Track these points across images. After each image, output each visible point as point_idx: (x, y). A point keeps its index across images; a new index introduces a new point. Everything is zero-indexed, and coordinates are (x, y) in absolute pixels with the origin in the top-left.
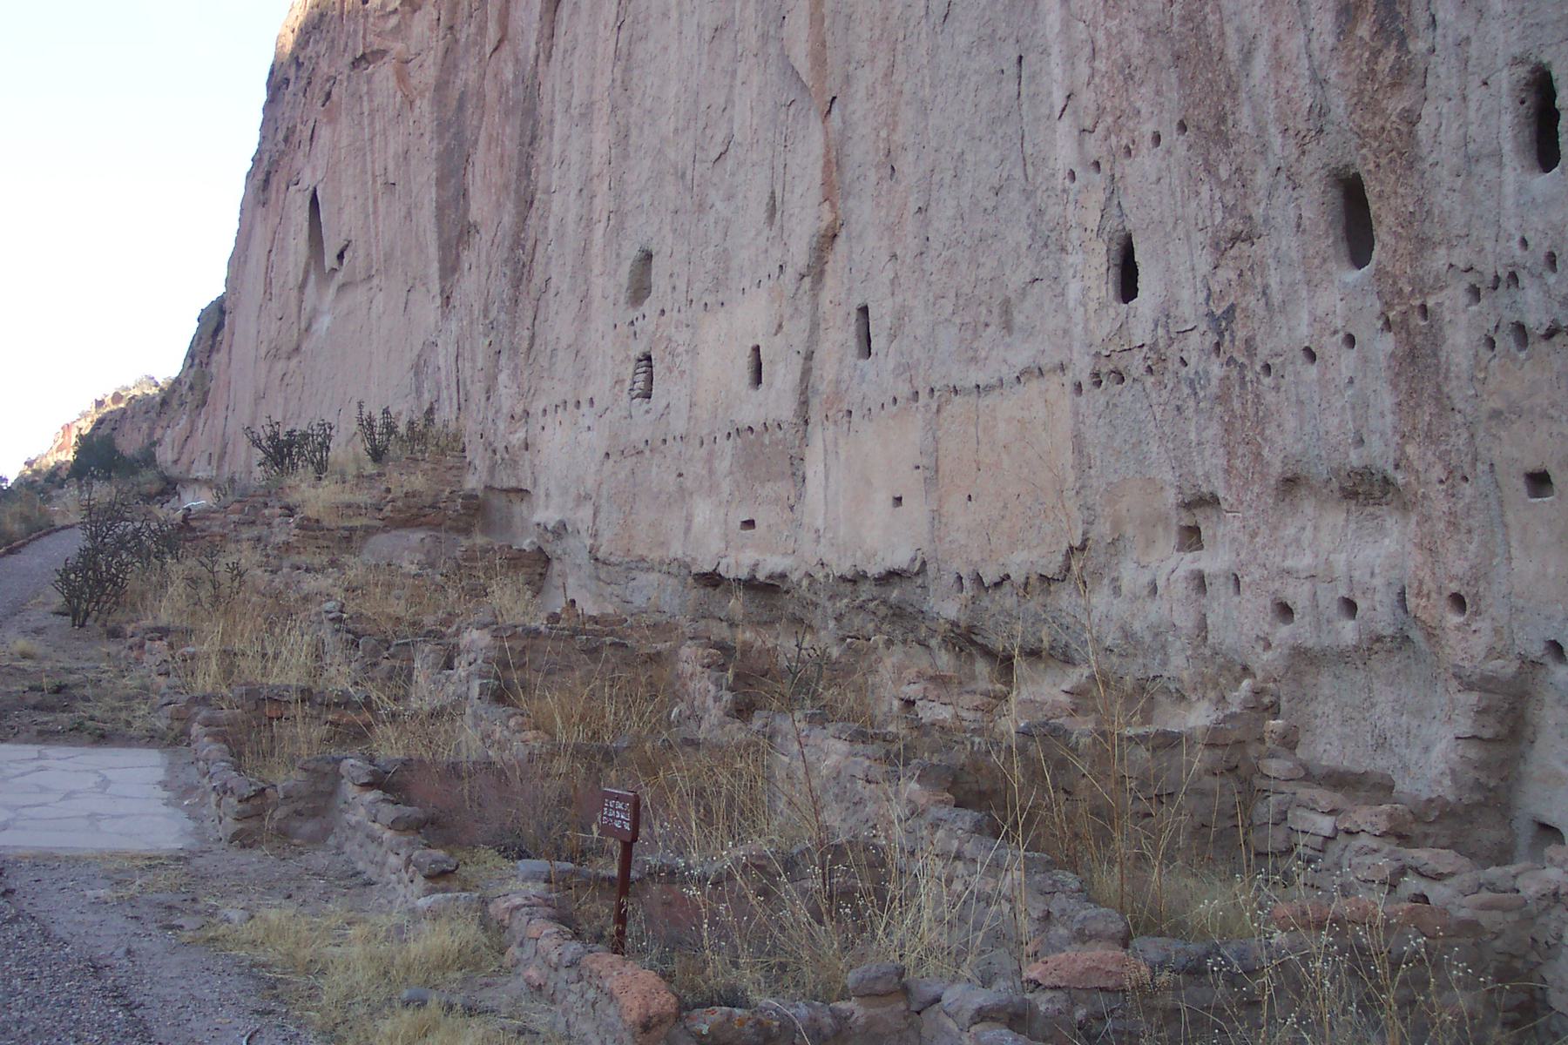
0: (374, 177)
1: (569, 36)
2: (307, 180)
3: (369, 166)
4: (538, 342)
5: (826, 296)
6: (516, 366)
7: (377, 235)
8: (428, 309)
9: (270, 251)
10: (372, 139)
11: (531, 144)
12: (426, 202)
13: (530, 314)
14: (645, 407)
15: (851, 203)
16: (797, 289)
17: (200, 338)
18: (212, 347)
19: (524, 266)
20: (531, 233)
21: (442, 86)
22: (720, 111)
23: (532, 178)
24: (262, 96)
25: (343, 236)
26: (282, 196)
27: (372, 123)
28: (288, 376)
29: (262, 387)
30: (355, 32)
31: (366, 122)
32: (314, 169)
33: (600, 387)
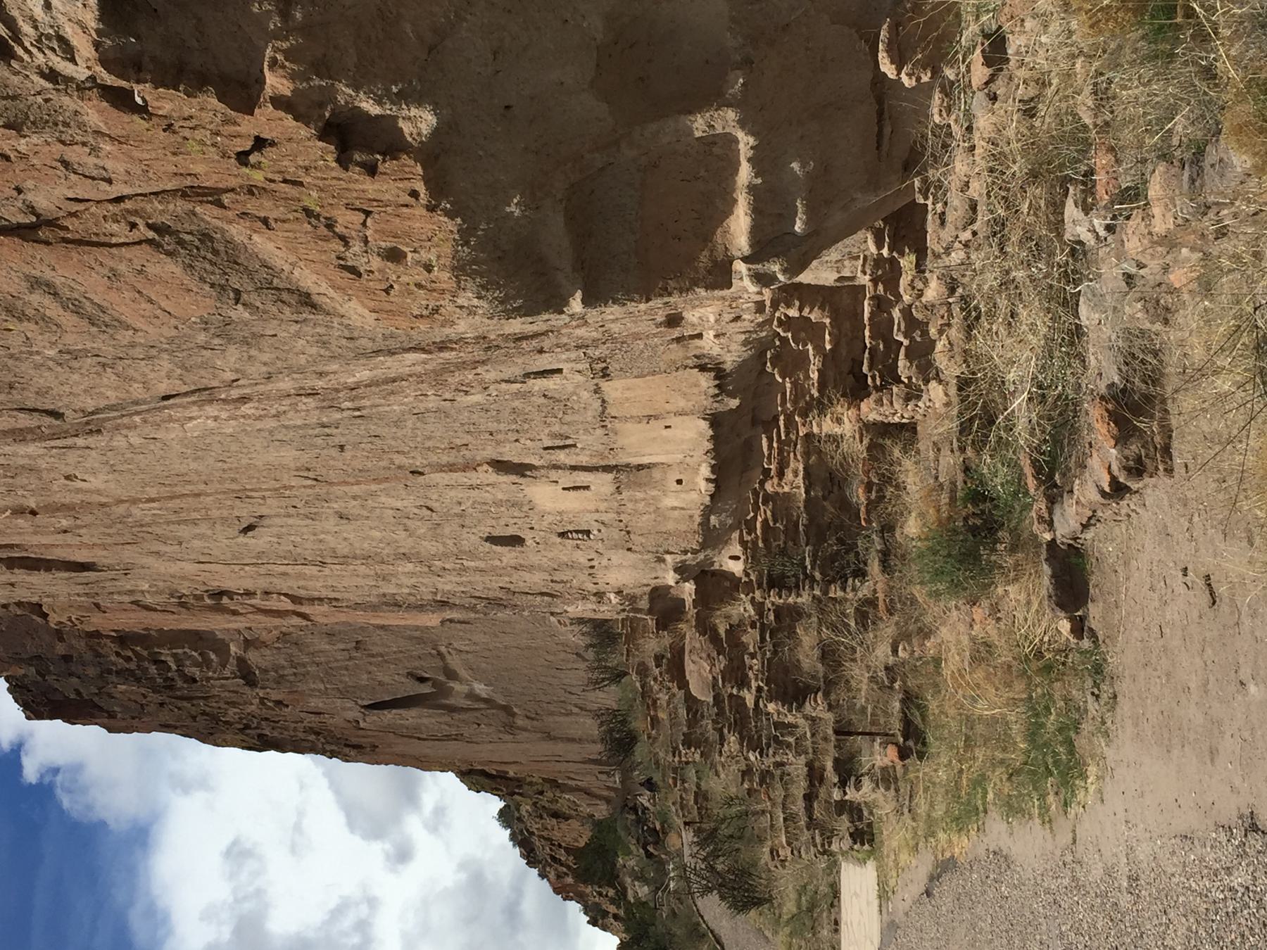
0: (351, 658)
1: (321, 589)
2: (354, 714)
4: (544, 590)
5: (536, 462)
9: (419, 739)
15: (478, 458)
17: (493, 789)
18: (501, 777)
24: (272, 755)
26: (370, 733)
27: (304, 665)
28: (528, 714)
29: (539, 735)
30: (222, 686)
32: (344, 709)
33: (581, 558)
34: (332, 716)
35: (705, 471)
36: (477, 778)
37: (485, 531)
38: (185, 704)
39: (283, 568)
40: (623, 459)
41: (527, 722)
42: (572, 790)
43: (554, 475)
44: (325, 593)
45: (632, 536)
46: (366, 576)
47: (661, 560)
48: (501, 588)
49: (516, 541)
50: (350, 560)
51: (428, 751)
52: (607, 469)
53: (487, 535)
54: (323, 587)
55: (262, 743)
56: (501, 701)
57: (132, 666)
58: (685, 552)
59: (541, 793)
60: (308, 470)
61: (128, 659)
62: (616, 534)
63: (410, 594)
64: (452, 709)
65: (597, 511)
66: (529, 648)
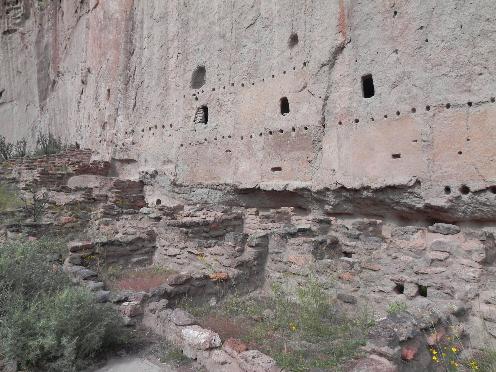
0: (13, 69)
3: (11, 66)
6: (127, 114)
7: (15, 87)
8: (35, 111)
10: (12, 58)
11: (132, 31)
12: (33, 78)
13: (134, 94)
14: (205, 126)
16: (319, 71)
19: (130, 76)
20: (133, 65)
21: (38, 42)
22: (250, 8)
23: (133, 43)
25: (2, 87)
27: (12, 53)
31: (9, 52)
33: (177, 120)
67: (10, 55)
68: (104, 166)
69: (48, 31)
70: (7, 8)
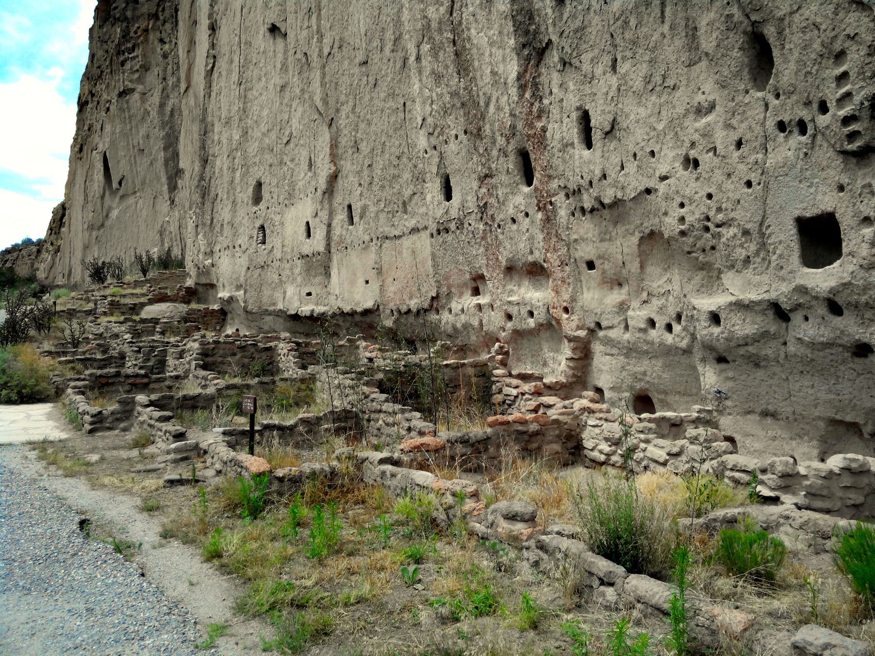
0: (134, 147)
2: (101, 148)
4: (215, 221)
8: (163, 206)
10: (131, 130)
21: (162, 105)
27: (130, 122)
30: (119, 80)
31: (127, 121)
33: (243, 240)
34: (101, 136)
35: (320, 309)
36: (60, 217)
37: (265, 180)
38: (107, 63)
39: (236, 59)
40: (335, 258)
41: (94, 237)
42: (53, 260)
43: (324, 215)
44: (215, 88)
45: (259, 271)
46: (229, 111)
47: (239, 287)
48: (217, 195)
49: (257, 198)
50: (242, 100)
51: (77, 186)
52: (328, 246)
53: (263, 181)
54: (221, 87)
55: (82, 104)
56: (108, 223)
57: (132, 34)
58: (245, 302)
59: (52, 244)
60: (340, 47)
61: (136, 33)
62: (261, 260)
63: (213, 141)
64: (103, 197)
65: (283, 246)
66: (138, 237)
67: (128, 128)
68: (186, 292)
69: (173, 89)
70: (122, 58)
